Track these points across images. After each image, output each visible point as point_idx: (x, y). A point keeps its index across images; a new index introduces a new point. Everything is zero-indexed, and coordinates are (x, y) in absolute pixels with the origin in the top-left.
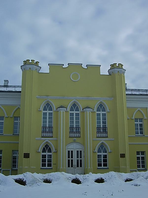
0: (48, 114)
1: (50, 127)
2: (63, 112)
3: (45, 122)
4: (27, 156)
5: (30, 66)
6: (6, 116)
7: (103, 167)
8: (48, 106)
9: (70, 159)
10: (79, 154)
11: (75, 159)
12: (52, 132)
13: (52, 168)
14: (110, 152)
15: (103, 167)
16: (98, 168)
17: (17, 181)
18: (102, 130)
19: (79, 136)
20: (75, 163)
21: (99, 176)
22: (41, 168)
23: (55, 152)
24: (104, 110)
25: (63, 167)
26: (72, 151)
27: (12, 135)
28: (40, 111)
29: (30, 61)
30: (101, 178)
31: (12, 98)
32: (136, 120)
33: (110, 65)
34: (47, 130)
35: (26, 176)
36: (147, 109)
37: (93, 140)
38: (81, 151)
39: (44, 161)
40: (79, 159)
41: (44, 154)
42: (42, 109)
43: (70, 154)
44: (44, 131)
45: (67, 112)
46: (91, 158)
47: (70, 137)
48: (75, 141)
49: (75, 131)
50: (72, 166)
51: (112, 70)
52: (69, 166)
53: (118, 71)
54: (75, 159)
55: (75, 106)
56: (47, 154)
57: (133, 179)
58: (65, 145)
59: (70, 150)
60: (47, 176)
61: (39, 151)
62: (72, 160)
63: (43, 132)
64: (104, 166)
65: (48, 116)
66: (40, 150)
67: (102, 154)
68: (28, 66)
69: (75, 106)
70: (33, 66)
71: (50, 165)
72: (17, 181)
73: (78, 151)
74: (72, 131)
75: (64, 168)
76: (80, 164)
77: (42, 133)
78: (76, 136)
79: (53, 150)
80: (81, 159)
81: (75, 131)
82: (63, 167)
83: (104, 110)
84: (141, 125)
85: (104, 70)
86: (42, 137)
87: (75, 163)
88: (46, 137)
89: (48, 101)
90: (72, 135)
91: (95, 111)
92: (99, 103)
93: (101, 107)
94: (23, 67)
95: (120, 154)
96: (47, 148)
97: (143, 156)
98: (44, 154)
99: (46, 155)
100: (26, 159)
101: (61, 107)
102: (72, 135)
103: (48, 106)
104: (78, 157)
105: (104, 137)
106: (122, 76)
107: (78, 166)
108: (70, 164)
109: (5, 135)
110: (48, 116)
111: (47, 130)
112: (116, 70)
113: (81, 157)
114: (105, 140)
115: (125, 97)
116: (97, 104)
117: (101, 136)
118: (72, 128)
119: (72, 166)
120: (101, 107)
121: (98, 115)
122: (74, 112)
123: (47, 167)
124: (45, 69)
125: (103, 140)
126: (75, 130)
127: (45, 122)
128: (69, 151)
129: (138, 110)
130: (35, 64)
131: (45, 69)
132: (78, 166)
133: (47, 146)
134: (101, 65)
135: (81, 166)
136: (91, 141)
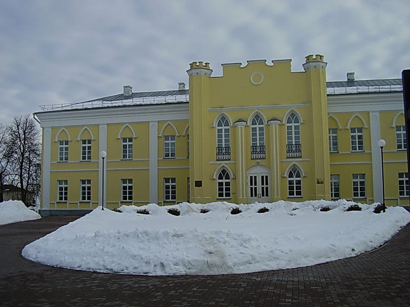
0: (223, 131)
1: (228, 148)
2: (241, 128)
3: (290, 138)
4: (198, 184)
5: (198, 71)
6: (177, 135)
7: (295, 196)
8: (223, 121)
9: (253, 186)
10: (265, 180)
11: (259, 186)
12: (229, 154)
13: (230, 199)
14: (305, 177)
15: (295, 196)
16: (289, 198)
17: (170, 211)
18: (294, 149)
19: (300, 156)
20: (259, 191)
21: (262, 206)
22: (218, 199)
23: (234, 178)
24: (297, 121)
25: (243, 197)
26: (255, 177)
27: (162, 159)
28: (213, 127)
29: (198, 64)
30: (179, 211)
31: (383, 101)
32: (353, 130)
33: (248, 61)
34: (224, 151)
35: (181, 207)
36: (369, 113)
37: (281, 162)
38: (267, 177)
39: (291, 188)
40: (265, 186)
41: (221, 181)
42: (215, 124)
43: (253, 180)
44: (289, 150)
45: (247, 126)
46: (278, 184)
47: (252, 159)
48: (258, 164)
49: (259, 151)
50: (256, 196)
51: (307, 65)
52: (252, 196)
53: (315, 66)
54: (259, 186)
55: (257, 119)
56: (224, 181)
57: (150, 213)
58: (244, 170)
59: (253, 175)
60: (205, 206)
61: (214, 177)
62: (256, 188)
63: (218, 154)
64: (361, 196)
65: (223, 134)
66: (216, 176)
67: (295, 179)
68: (194, 71)
69: (257, 119)
70: (200, 70)
71: (299, 193)
72: (170, 211)
73: (263, 177)
74: (255, 150)
75: (245, 197)
76: (265, 192)
77: (287, 152)
78: (257, 157)
79: (231, 176)
80: (267, 186)
81: (259, 151)
82: (243, 197)
83: (297, 121)
84: (360, 137)
85: (297, 66)
86: (217, 160)
87: (259, 191)
88: (222, 160)
89: (223, 114)
90: (255, 156)
91: (284, 123)
92: (290, 112)
93: (293, 117)
94: (190, 72)
95: (196, 181)
96: (224, 174)
97: (89, 185)
98: (221, 181)
99: (223, 183)
100: (199, 188)
101: (240, 121)
102: (221, 157)
103: (223, 121)
104: (263, 184)
105: (296, 157)
106: (321, 72)
107: (263, 195)
108: (254, 193)
109: (179, 158)
110: (223, 134)
111: (294, 149)
112: (314, 62)
113: (267, 184)
114: (299, 161)
115: (324, 99)
116: (286, 115)
117: (295, 156)
118: (254, 147)
119: (256, 196)
120: (293, 117)
121: (289, 128)
122: (223, 128)
123: (63, 201)
124: (218, 72)
125: (295, 161)
126: (258, 150)
127: (290, 138)
128: (251, 177)
129: (355, 115)
130: (204, 67)
131: (218, 72)
132: (263, 195)
133: (224, 171)
134: (291, 60)
135: (267, 195)
136: (278, 164)
